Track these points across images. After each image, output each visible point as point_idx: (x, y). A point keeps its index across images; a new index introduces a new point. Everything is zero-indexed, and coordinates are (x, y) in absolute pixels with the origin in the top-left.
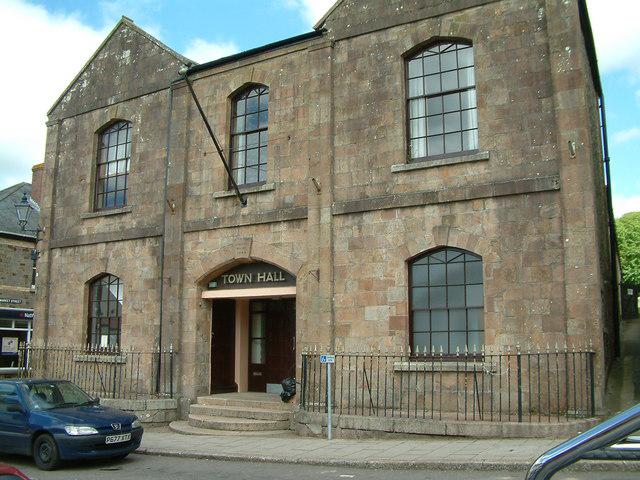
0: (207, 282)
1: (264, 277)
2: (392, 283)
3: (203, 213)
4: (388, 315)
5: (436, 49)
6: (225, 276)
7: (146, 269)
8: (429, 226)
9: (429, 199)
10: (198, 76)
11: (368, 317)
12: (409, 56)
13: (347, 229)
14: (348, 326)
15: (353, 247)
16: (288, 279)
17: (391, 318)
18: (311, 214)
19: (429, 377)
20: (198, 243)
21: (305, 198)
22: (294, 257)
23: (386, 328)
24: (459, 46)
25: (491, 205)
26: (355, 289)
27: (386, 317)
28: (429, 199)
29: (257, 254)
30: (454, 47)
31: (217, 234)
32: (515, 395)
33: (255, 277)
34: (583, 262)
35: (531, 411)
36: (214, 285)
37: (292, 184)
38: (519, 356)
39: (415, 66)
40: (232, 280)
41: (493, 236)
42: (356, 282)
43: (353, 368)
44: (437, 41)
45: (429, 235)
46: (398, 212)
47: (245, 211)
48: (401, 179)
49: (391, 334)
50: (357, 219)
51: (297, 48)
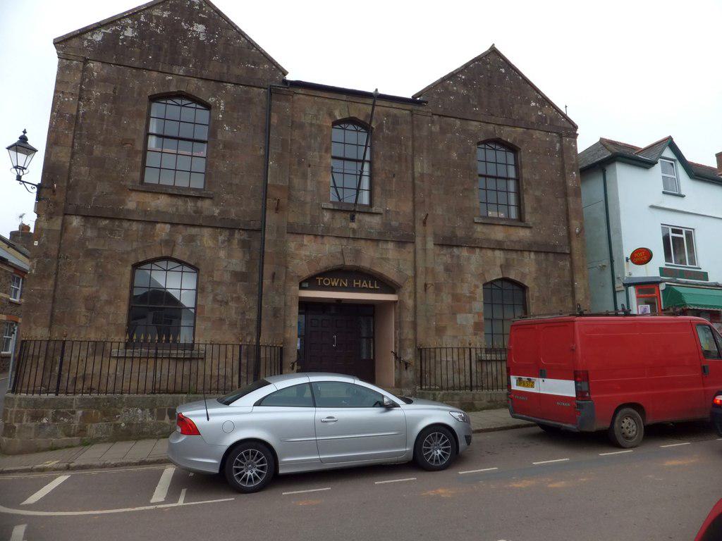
0: (312, 282)
1: (359, 283)
2: (475, 299)
3: (309, 218)
4: (473, 321)
5: (179, 101)
6: (319, 279)
7: (234, 261)
8: (498, 262)
9: (499, 246)
10: (300, 91)
11: (459, 321)
12: (154, 98)
13: (445, 257)
14: (445, 327)
15: (447, 269)
16: (386, 285)
17: (475, 323)
18: (418, 240)
19: (187, 363)
20: (302, 245)
21: (414, 228)
22: (399, 271)
23: (471, 330)
24: (198, 106)
25: (532, 255)
26: (450, 300)
27: (471, 322)
28: (499, 246)
29: (365, 264)
30: (194, 105)
31: (326, 240)
32: (468, 378)
33: (351, 283)
34: (583, 297)
35: (477, 386)
36: (306, 285)
37: (397, 213)
38: (240, 346)
39: (157, 109)
40: (327, 282)
41: (534, 275)
42: (450, 295)
43: (449, 359)
44: (180, 95)
45: (498, 270)
46: (478, 250)
47: (354, 225)
48: (479, 228)
49: (475, 334)
50: (449, 250)
51: (401, 106)
